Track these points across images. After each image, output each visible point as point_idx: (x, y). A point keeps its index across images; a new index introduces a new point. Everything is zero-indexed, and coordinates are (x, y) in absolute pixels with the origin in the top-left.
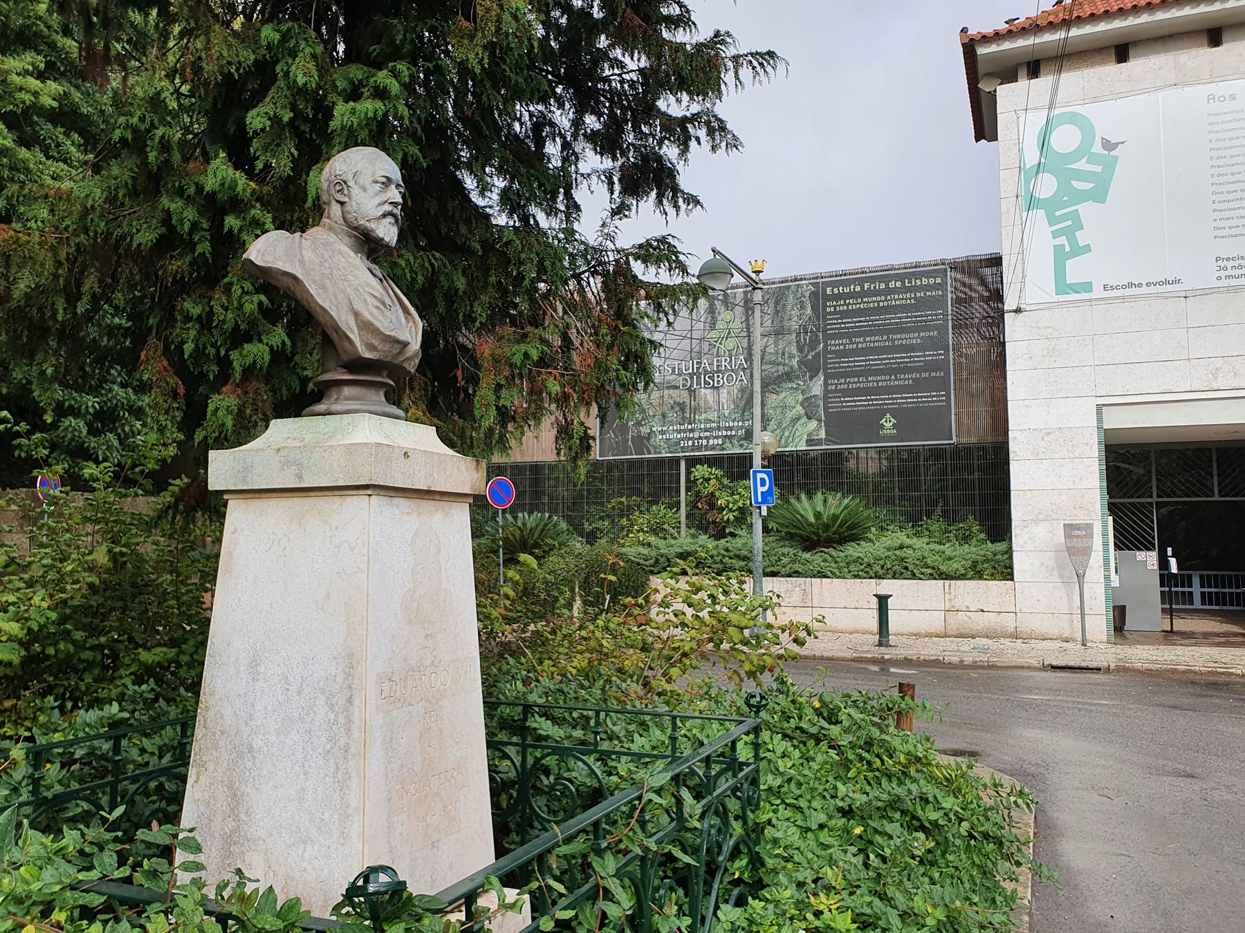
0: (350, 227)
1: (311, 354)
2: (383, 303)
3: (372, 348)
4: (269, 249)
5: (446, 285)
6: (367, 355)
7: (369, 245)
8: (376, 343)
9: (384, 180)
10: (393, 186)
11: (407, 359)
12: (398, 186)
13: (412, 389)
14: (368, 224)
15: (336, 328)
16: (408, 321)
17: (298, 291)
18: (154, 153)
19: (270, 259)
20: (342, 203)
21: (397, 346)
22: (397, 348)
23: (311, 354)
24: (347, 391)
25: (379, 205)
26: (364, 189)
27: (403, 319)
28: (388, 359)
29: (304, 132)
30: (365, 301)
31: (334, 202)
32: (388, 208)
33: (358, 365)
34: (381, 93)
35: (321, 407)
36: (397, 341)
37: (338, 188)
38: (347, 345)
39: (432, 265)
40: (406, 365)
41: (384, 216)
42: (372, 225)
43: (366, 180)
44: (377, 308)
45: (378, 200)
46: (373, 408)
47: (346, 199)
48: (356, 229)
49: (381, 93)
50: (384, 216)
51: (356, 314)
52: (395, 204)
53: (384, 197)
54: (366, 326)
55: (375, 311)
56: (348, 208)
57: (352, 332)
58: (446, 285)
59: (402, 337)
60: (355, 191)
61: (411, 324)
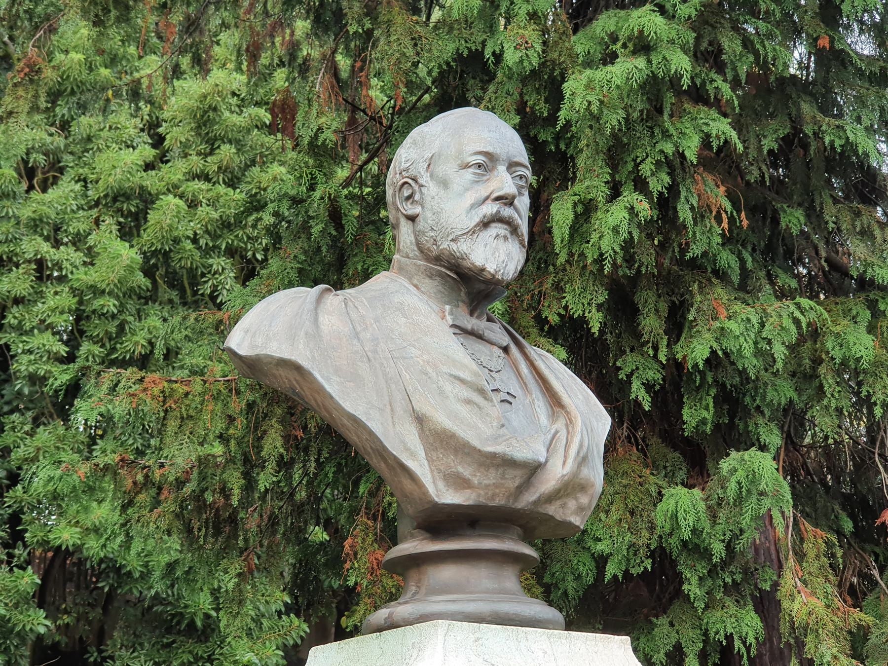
0: (428, 259)
1: (607, 512)
2: (481, 392)
3: (458, 482)
4: (275, 325)
5: (838, 354)
6: (449, 497)
7: (468, 287)
8: (466, 471)
9: (480, 159)
10: (502, 168)
11: (550, 498)
12: (512, 166)
13: (800, 556)
14: (454, 246)
15: (383, 453)
16: (553, 417)
17: (307, 393)
18: (320, 227)
19: (259, 341)
20: (412, 219)
21: (511, 473)
22: (514, 479)
23: (607, 512)
24: (447, 573)
25: (473, 206)
26: (444, 184)
27: (544, 419)
28: (499, 501)
29: (545, 142)
30: (441, 392)
31: (403, 222)
32: (491, 208)
33: (442, 522)
34: (643, 46)
35: (400, 610)
36: (507, 463)
37: (406, 193)
38: (407, 484)
39: (797, 322)
40: (553, 510)
41: (485, 224)
42: (462, 247)
43: (447, 169)
44: (468, 402)
45: (471, 197)
46: (470, 607)
47: (417, 210)
48: (438, 260)
49: (643, 46)
50: (485, 224)
51: (420, 420)
52: (507, 200)
53: (483, 191)
54: (441, 441)
55: (463, 411)
56: (421, 224)
57: (413, 455)
58: (838, 354)
59: (522, 452)
60: (431, 189)
61: (560, 424)
